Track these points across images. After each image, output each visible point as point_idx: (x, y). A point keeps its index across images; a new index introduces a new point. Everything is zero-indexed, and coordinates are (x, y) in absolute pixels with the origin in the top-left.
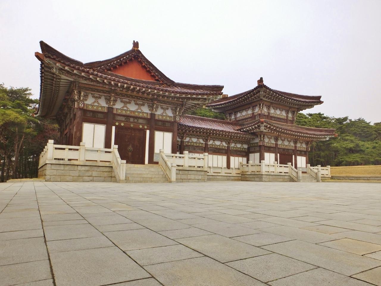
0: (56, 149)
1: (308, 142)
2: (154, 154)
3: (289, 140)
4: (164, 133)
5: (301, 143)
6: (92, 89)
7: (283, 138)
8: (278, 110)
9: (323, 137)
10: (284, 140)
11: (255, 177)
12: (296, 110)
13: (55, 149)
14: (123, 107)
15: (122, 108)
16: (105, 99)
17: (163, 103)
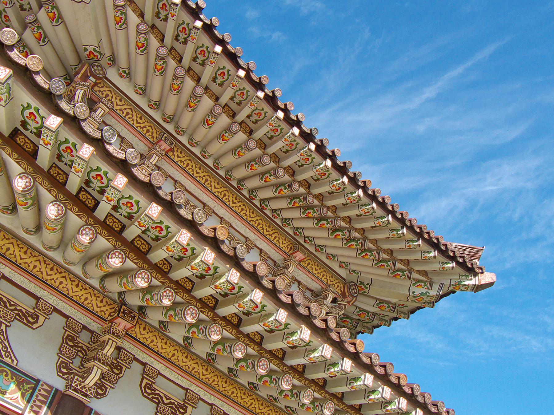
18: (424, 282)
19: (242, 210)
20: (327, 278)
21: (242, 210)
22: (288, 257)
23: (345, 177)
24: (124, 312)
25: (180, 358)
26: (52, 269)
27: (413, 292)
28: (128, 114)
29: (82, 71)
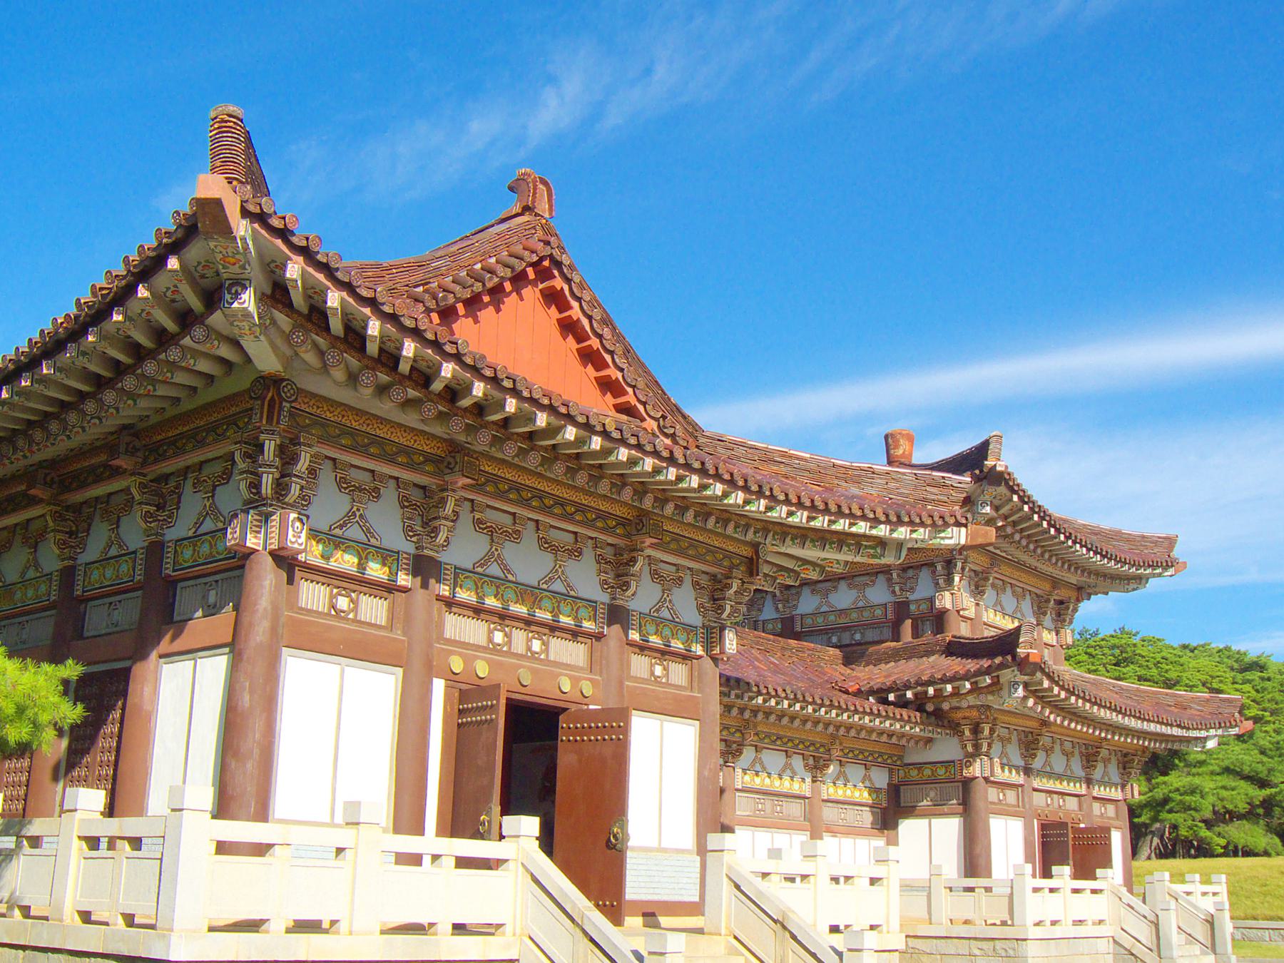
0: (223, 848)
1: (1126, 755)
2: (629, 854)
4: (343, 671)
6: (353, 433)
11: (977, 952)
12: (1074, 595)
13: (397, 863)
14: (484, 562)
15: (482, 566)
16: (403, 507)
17: (599, 524)
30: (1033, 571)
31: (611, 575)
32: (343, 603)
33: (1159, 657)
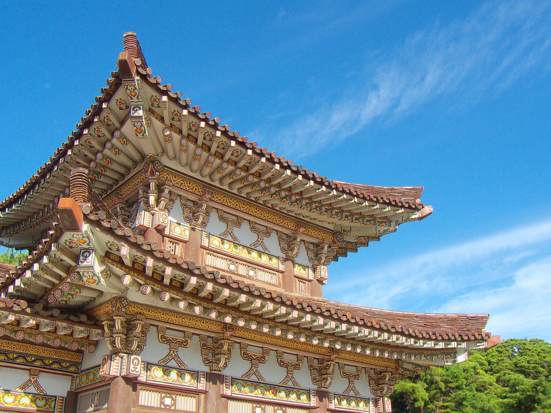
3: (290, 359)
5: (351, 378)
7: (254, 351)
8: (245, 226)
9: (441, 345)
10: (261, 360)
14: (247, 374)
18: (385, 222)
19: (262, 214)
20: (321, 235)
21: (262, 214)
22: (296, 232)
23: (323, 187)
24: (229, 328)
25: (258, 337)
26: (190, 320)
27: (379, 231)
28: (182, 184)
29: (149, 170)
30: (280, 213)
31: (211, 355)
32: (168, 401)
33: (539, 349)
